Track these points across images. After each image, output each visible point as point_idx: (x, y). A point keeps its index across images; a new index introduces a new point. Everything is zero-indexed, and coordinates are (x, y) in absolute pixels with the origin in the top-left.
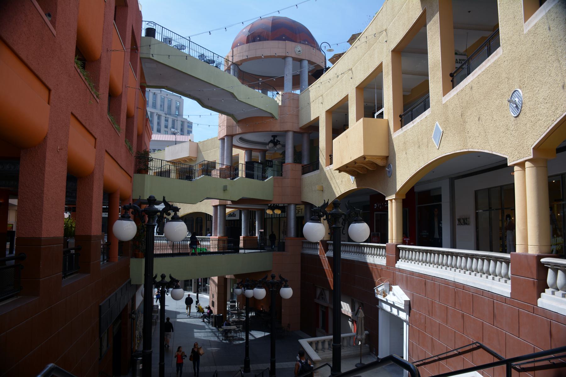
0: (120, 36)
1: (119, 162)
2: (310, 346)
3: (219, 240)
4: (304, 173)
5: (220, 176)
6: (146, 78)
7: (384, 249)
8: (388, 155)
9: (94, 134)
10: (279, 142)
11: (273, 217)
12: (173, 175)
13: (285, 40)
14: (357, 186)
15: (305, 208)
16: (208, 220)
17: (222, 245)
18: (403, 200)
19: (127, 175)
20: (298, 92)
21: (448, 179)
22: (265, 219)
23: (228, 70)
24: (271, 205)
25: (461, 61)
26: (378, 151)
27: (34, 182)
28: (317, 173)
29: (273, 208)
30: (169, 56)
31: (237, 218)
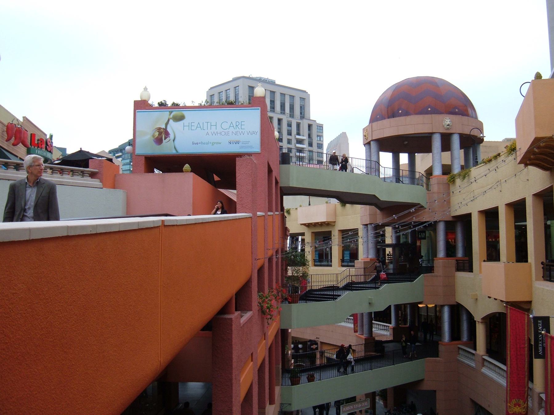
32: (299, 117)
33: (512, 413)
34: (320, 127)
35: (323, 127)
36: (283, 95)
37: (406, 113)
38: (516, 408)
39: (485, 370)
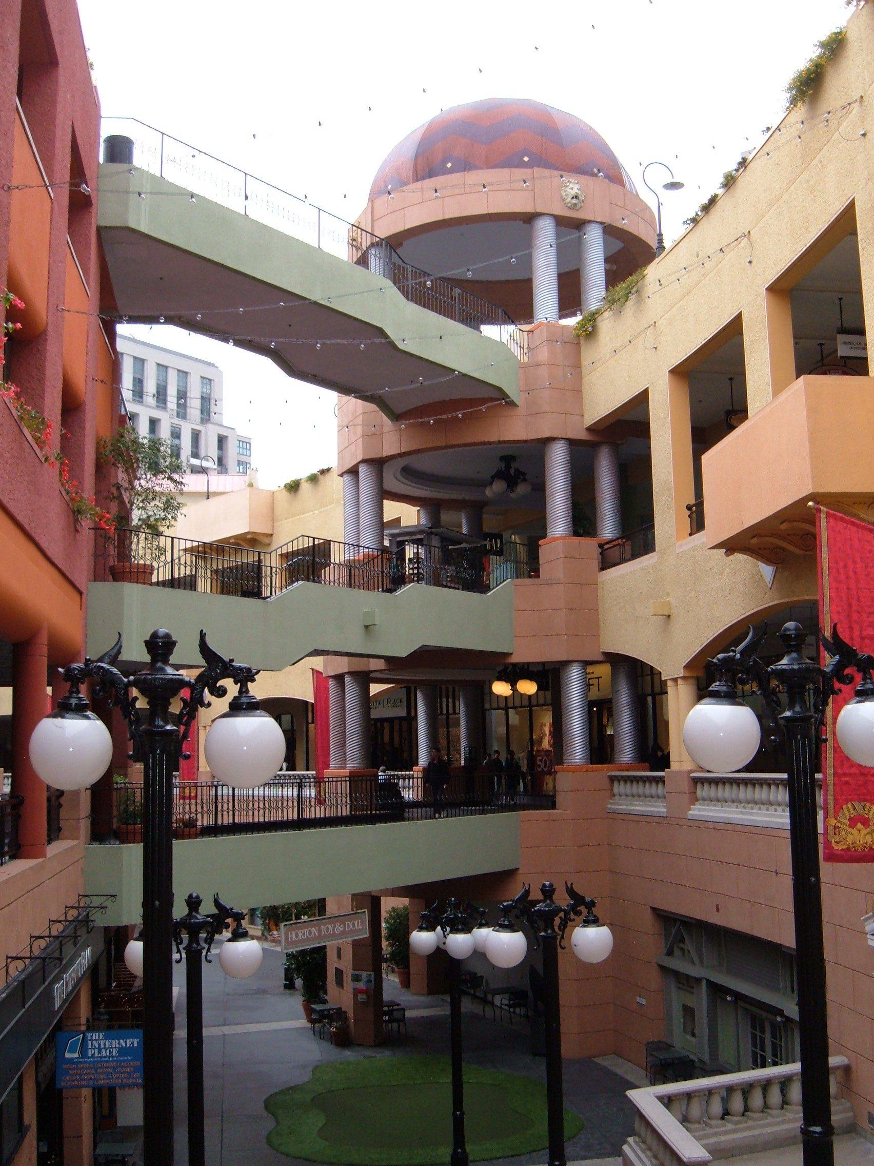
2: (666, 1110)
4: (605, 565)
11: (510, 704)
12: (204, 585)
16: (310, 721)
28: (651, 562)
29: (513, 674)
32: (199, 420)
33: (845, 847)
34: (245, 444)
35: (250, 444)
36: (162, 368)
37: (466, 166)
38: (854, 831)
39: (699, 811)
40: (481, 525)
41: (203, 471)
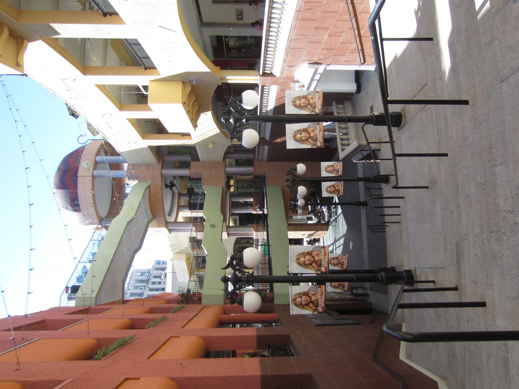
0: (76, 323)
1: (192, 317)
3: (257, 231)
4: (198, 160)
5: (202, 231)
6: (116, 300)
7: (264, 87)
8: (182, 82)
9: (167, 339)
10: (171, 181)
13: (77, 177)
14: (209, 110)
15: (228, 158)
16: (240, 243)
17: (261, 228)
18: (221, 69)
19: (202, 310)
20: (126, 165)
21: (202, 28)
22: (238, 194)
23: (106, 228)
24: (226, 188)
25: (91, 8)
26: (177, 90)
27: (211, 386)
28: (198, 147)
29: (228, 186)
30: (8, 96)
31: (237, 217)
34: (158, 263)
40: (185, 194)
41: (166, 275)
